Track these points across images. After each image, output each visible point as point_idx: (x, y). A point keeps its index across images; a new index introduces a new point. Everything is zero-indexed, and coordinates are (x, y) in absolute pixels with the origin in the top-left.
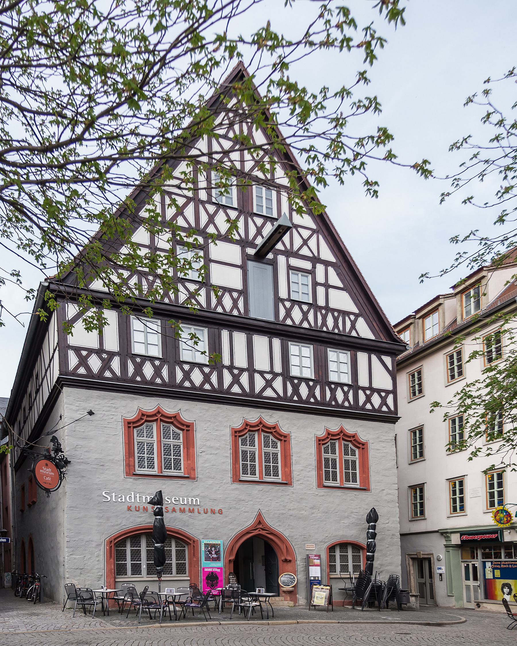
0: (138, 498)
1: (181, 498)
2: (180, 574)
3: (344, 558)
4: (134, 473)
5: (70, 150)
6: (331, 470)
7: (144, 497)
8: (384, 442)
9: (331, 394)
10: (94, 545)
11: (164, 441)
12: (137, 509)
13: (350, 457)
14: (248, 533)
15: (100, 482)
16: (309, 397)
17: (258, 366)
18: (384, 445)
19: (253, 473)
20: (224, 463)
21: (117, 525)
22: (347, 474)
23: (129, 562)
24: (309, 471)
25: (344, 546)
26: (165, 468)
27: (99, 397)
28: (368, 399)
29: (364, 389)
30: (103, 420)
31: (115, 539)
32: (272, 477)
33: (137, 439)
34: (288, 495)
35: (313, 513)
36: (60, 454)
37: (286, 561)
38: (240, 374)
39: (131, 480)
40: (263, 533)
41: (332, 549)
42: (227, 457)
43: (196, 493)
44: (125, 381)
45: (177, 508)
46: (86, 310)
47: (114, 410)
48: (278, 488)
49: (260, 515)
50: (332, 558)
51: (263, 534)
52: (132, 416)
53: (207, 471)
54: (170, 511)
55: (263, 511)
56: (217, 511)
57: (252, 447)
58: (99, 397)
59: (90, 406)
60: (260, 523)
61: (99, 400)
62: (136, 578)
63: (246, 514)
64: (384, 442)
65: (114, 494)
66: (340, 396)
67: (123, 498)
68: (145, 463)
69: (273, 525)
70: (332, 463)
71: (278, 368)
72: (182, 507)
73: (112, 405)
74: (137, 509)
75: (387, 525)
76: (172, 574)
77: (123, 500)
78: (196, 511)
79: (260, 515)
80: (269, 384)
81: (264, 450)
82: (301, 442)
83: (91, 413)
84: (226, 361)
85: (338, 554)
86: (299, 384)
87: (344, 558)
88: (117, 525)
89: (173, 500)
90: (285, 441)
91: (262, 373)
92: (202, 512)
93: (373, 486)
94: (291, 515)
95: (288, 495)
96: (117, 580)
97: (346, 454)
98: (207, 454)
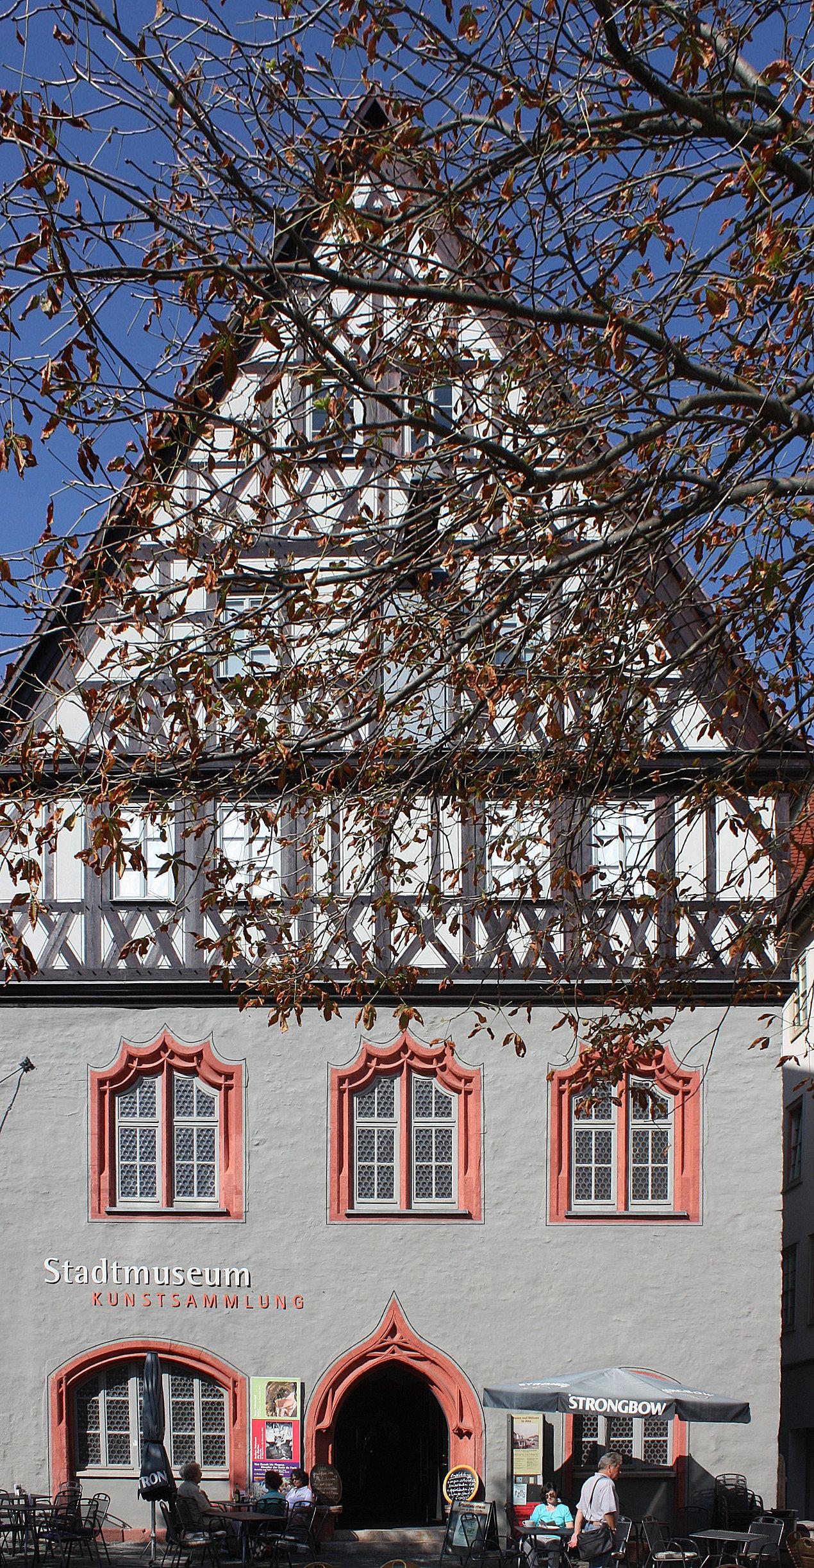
0: (115, 1271)
1: (207, 1270)
2: (211, 1463)
4: (570, 1213)
5: (785, 393)
6: (593, 1165)
7: (127, 1271)
8: (747, 1065)
9: (644, 938)
10: (28, 1390)
11: (418, 1122)
12: (114, 1301)
13: (433, 1122)
14: (363, 1359)
15: (41, 1236)
16: (532, 954)
18: (750, 1077)
19: (387, 1192)
20: (310, 1168)
21: (72, 1341)
22: (640, 1174)
23: (102, 1431)
24: (530, 1175)
26: (360, 1194)
27: (43, 1022)
28: (702, 938)
29: (693, 907)
30: (50, 1079)
31: (69, 1375)
32: (434, 1199)
33: (121, 1122)
34: (469, 1248)
35: (533, 1298)
37: (461, 1433)
39: (101, 1227)
40: (402, 1356)
42: (318, 1151)
43: (242, 1254)
44: (94, 974)
45: (199, 1296)
46: (711, 811)
47: (71, 1051)
48: (443, 1229)
49: (394, 1307)
51: (402, 1359)
52: (111, 1065)
53: (270, 1194)
54: (184, 1304)
55: (403, 1298)
56: (290, 1301)
57: (148, 1119)
58: (45, 1022)
59: (25, 1048)
60: (393, 1331)
61: (43, 1030)
62: (118, 1470)
63: (360, 1306)
64: (747, 1065)
65: (66, 1266)
66: (520, 943)
68: (135, 1183)
69: (429, 1334)
70: (598, 1145)
72: (211, 1293)
73: (69, 1039)
74: (114, 1301)
75: (743, 1321)
76: (98, 1461)
77: (85, 1280)
78: (242, 1301)
79: (394, 1307)
81: (636, 1124)
82: (510, 1090)
83: (28, 1066)
84: (320, 887)
86: (608, 920)
88: (72, 1341)
89: (189, 1273)
90: (686, 1093)
92: (256, 1303)
93: (708, 1205)
94: (475, 1306)
95: (469, 1248)
96: (79, 1474)
97: (424, 1111)
98: (269, 1149)
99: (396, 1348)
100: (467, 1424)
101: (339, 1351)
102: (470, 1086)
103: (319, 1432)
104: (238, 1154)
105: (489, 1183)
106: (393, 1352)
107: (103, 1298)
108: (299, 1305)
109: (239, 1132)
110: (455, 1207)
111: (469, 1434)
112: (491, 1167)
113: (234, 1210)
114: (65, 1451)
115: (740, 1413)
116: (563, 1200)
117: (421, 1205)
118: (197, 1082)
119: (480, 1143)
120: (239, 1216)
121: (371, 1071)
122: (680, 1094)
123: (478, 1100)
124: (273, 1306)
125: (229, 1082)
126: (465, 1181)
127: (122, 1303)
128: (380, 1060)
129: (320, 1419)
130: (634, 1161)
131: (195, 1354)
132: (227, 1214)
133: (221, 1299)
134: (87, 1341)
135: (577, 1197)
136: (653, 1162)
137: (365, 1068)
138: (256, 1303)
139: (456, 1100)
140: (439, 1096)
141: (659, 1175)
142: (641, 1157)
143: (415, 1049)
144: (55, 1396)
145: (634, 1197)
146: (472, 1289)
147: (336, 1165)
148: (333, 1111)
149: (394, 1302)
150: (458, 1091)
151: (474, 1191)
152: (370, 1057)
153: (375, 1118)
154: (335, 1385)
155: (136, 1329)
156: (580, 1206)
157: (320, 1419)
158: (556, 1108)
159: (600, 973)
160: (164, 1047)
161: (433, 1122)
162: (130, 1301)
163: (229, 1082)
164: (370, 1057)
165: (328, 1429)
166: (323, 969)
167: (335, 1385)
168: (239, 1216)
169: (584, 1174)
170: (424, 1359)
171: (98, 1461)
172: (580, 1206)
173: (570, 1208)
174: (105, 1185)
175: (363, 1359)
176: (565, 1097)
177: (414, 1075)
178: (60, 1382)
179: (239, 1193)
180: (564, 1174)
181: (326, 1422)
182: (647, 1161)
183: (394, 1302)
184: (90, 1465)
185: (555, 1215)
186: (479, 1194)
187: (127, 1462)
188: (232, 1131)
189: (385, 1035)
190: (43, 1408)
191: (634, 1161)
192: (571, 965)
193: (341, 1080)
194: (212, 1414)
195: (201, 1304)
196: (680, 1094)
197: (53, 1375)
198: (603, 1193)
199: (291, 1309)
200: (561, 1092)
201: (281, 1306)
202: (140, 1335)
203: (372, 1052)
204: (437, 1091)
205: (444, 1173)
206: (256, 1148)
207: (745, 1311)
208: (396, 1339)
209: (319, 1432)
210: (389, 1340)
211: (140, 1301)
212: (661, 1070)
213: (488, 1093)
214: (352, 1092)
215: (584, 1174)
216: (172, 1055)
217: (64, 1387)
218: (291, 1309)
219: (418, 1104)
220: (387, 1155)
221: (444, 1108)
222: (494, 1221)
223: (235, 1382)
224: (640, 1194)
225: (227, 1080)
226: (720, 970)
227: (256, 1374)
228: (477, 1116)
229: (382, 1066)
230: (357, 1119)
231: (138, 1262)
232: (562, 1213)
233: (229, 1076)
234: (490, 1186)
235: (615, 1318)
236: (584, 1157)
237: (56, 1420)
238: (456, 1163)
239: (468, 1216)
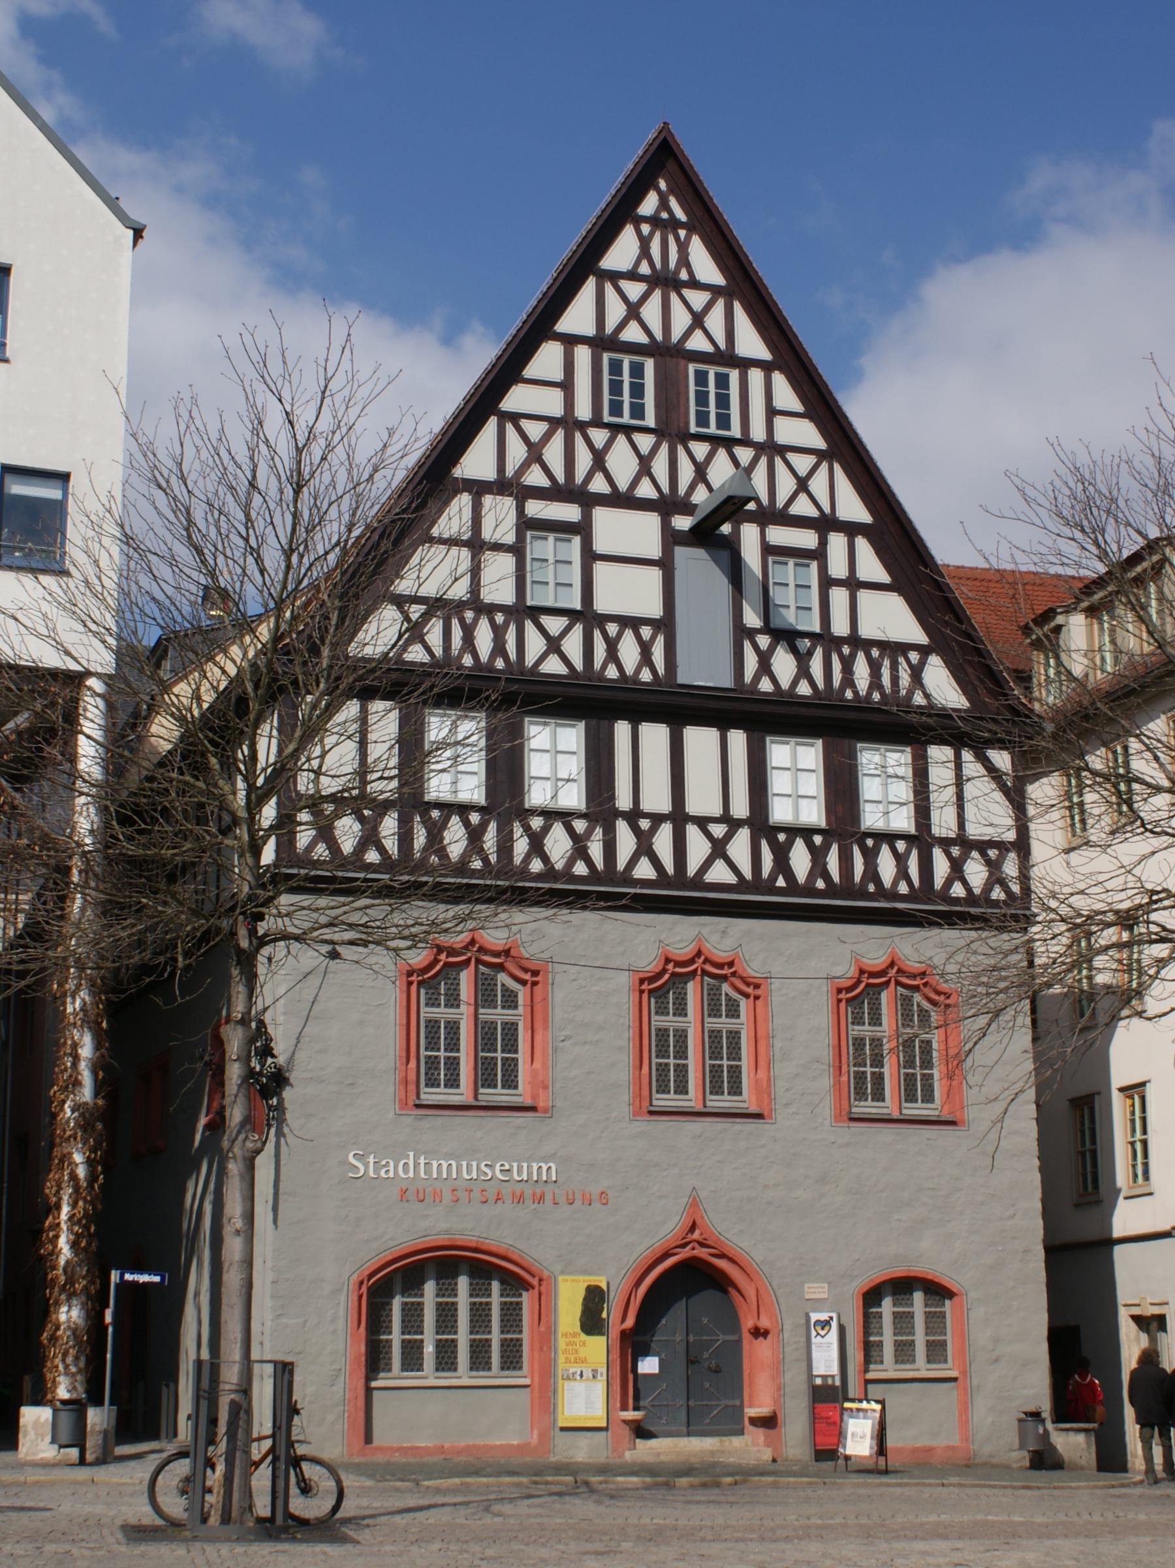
0: (422, 1166)
1: (515, 1165)
2: (508, 1369)
3: (903, 1321)
4: (417, 1102)
6: (725, 1062)
13: (723, 1023)
14: (666, 1255)
17: (693, 807)
19: (682, 1089)
22: (716, 1071)
23: (396, 1337)
25: (902, 1286)
31: (370, 1276)
34: (763, 1146)
36: (270, 1060)
38: (654, 829)
39: (408, 1120)
40: (702, 1253)
41: (872, 1297)
42: (620, 1048)
45: (506, 1191)
48: (738, 1127)
49: (694, 1204)
50: (869, 1321)
54: (492, 1198)
55: (703, 1194)
56: (595, 1197)
67: (391, 1168)
71: (740, 808)
74: (421, 1196)
77: (391, 1175)
78: (548, 1197)
79: (694, 1204)
80: (719, 849)
84: (624, 801)
85: (887, 1306)
87: (903, 1321)
89: (498, 1168)
91: (702, 822)
92: (562, 1199)
95: (763, 1146)
99: (696, 1245)
100: (764, 1323)
101: (642, 1248)
102: (758, 992)
103: (623, 1333)
104: (545, 1050)
105: (779, 1084)
106: (693, 1249)
107: (411, 1195)
108: (604, 1201)
109: (546, 1028)
110: (885, 1111)
111: (765, 1334)
112: (782, 1070)
113: (541, 1104)
114: (363, 1359)
115: (1125, 1305)
116: (845, 1103)
117: (490, 1095)
118: (502, 978)
119: (769, 1046)
120: (546, 1111)
121: (441, 963)
122: (529, 985)
123: (766, 1004)
124: (578, 1203)
125: (534, 979)
126: (757, 1081)
127: (428, 1200)
128: (678, 964)
129: (624, 1318)
130: (657, 1057)
131: (501, 1251)
132: (533, 1109)
133: (528, 1193)
134: (392, 1239)
135: (711, 1093)
136: (446, 1050)
137: (664, 971)
138: (562, 1199)
139: (744, 1004)
140: (921, 1010)
141: (433, 1063)
142: (716, 1054)
143: (709, 955)
144: (356, 1298)
145: (711, 1093)
146: (766, 1187)
147: (638, 1062)
148: (634, 1011)
149: (694, 1199)
150: (747, 996)
151: (765, 1089)
152: (668, 960)
153: (671, 1017)
154: (638, 1284)
155: (443, 1226)
156: (431, 1095)
157: (624, 1318)
158: (405, 995)
159: (431, 871)
160: (699, 953)
161: (723, 1023)
162: (437, 1196)
163: (534, 979)
164: (668, 960)
165: (631, 1329)
166: (698, 882)
167: (638, 1284)
168: (546, 1111)
169: (663, 1069)
170: (722, 1256)
171: (390, 1370)
172: (431, 1095)
173: (418, 1097)
174: (412, 1076)
175: (666, 1255)
176: (414, 988)
177: (706, 978)
178: (361, 1283)
179: (546, 1087)
180: (413, 1064)
181: (630, 1322)
182: (722, 1059)
183: (694, 1199)
184: (382, 1375)
185: (838, 1118)
186: (769, 1095)
187: (420, 1369)
188: (538, 1024)
189: (681, 941)
190: (342, 1312)
191: (657, 1057)
192: (847, 888)
193: (642, 981)
194: (511, 1317)
195: (508, 1200)
196: (529, 985)
197: (355, 1276)
198: (453, 1082)
199: (596, 1205)
200: (410, 983)
201: (586, 1203)
202: (447, 1232)
203: (670, 956)
204: (503, 985)
205: (735, 1072)
206: (561, 1044)
207: (1010, 1212)
208: (696, 1235)
209: (623, 1333)
210: (691, 1237)
211: (447, 1197)
212: (925, 984)
213: (776, 999)
214: (420, 983)
215: (433, 1063)
216: (706, 961)
217: (364, 1289)
218: (596, 1205)
219: (485, 994)
220: (682, 1053)
221: (733, 1012)
222: (785, 1120)
223: (540, 1280)
224: (717, 1089)
225: (533, 975)
226: (550, 873)
227: (562, 1273)
228: (766, 1021)
229: (678, 970)
230: (654, 1018)
231: (447, 1157)
232: (411, 1103)
233: (535, 973)
234: (780, 1086)
235: (896, 1217)
236: (432, 1044)
237: (356, 1325)
238: (745, 1063)
239: (759, 1116)
